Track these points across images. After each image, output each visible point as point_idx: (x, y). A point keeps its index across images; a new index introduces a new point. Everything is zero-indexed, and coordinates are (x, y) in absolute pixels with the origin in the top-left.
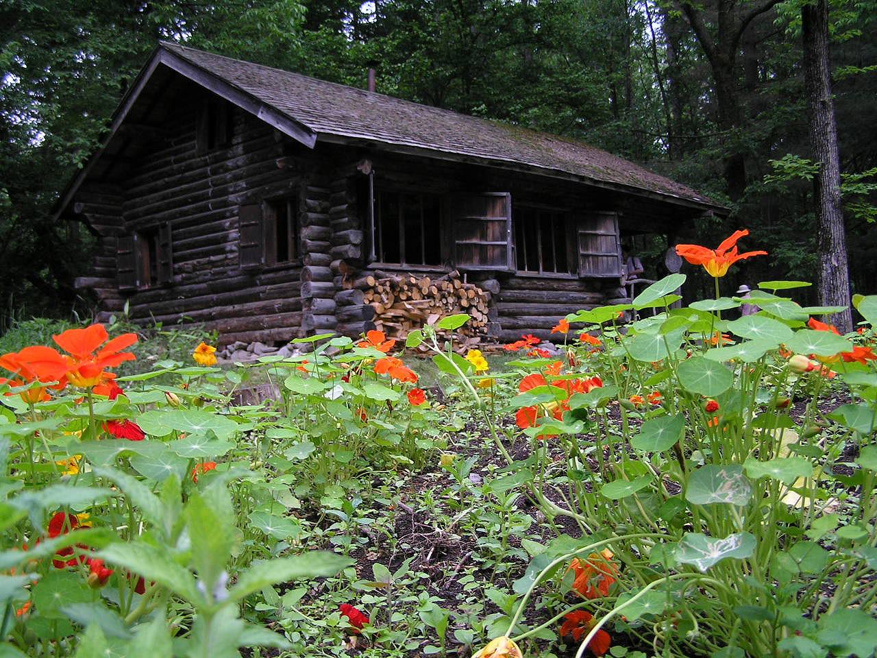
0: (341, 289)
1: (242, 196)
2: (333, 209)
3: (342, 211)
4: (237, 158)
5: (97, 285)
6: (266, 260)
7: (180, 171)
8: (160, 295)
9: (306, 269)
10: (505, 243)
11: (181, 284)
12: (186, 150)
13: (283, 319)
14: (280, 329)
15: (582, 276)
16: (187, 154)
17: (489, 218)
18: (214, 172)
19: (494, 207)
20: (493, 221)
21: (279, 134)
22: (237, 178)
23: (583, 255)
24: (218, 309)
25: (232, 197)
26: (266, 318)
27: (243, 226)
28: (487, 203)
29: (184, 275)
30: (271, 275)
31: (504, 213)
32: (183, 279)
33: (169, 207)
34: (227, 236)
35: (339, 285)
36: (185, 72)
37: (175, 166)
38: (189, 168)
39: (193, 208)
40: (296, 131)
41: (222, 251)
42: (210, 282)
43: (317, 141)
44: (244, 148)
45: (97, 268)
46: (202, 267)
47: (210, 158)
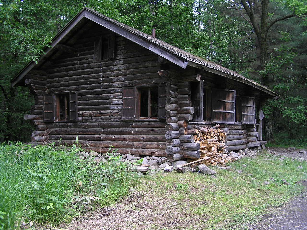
0: (183, 134)
1: (122, 84)
2: (179, 96)
3: (186, 98)
4: (119, 65)
5: (35, 118)
6: (136, 116)
7: (82, 68)
8: (68, 125)
9: (169, 125)
10: (233, 112)
11: (81, 121)
12: (87, 59)
13: (146, 145)
14: (143, 150)
15: (243, 123)
16: (87, 61)
17: (227, 101)
18: (104, 71)
19: (229, 97)
20: (228, 102)
21: (162, 59)
22: (118, 75)
23: (243, 115)
24: (105, 136)
25: (115, 84)
26: (135, 143)
27: (124, 99)
28: (226, 95)
29: (83, 117)
30: (139, 123)
31: (233, 99)
32: (83, 119)
33: (75, 84)
34: (112, 102)
35: (182, 132)
36: (100, 22)
37: (80, 66)
38: (88, 67)
39: (90, 87)
40: (174, 59)
41: (108, 109)
42: (100, 123)
43: (187, 65)
44: (124, 61)
45: (35, 110)
46: (96, 115)
47: (102, 64)
